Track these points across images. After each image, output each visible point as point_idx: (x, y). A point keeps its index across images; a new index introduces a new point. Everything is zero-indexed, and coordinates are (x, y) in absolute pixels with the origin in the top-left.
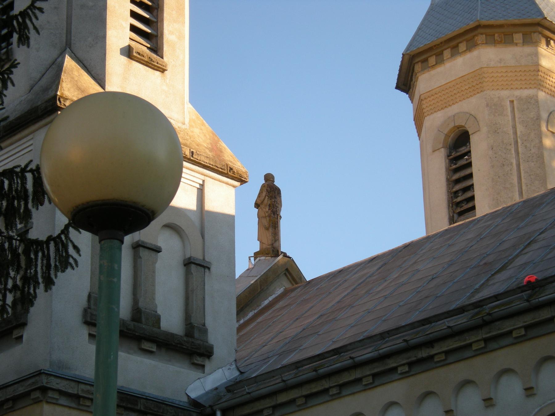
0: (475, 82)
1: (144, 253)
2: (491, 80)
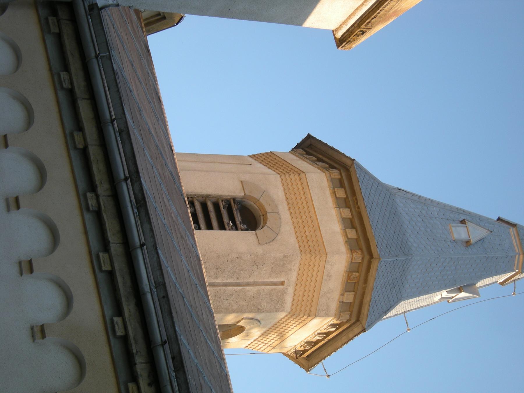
0: (312, 245)
2: (311, 264)
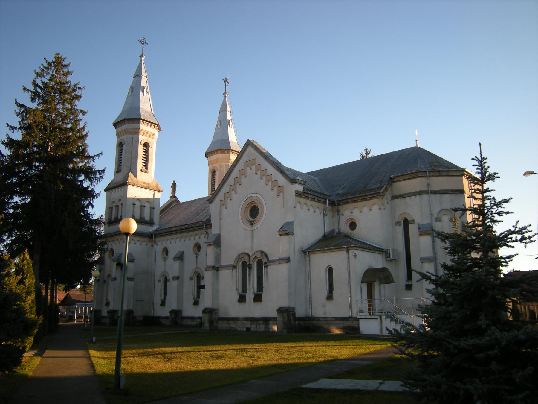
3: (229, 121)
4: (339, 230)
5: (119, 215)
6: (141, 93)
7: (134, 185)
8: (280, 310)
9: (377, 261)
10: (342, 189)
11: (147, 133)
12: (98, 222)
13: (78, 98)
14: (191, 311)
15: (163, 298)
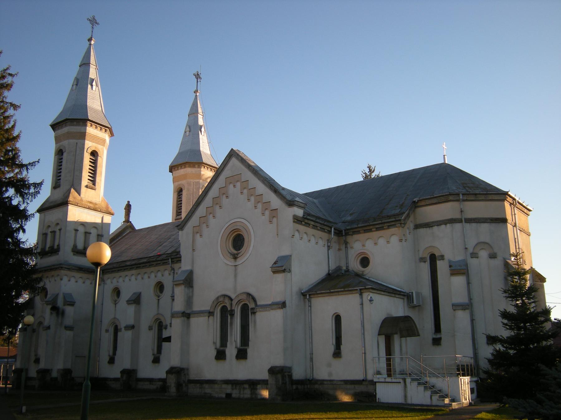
1: (87, 234)
3: (201, 127)
4: (347, 267)
5: (56, 244)
6: (89, 86)
7: (76, 205)
8: (272, 371)
9: (398, 308)
10: (351, 214)
11: (95, 138)
12: (29, 252)
13: (8, 87)
14: (148, 370)
15: (111, 353)
